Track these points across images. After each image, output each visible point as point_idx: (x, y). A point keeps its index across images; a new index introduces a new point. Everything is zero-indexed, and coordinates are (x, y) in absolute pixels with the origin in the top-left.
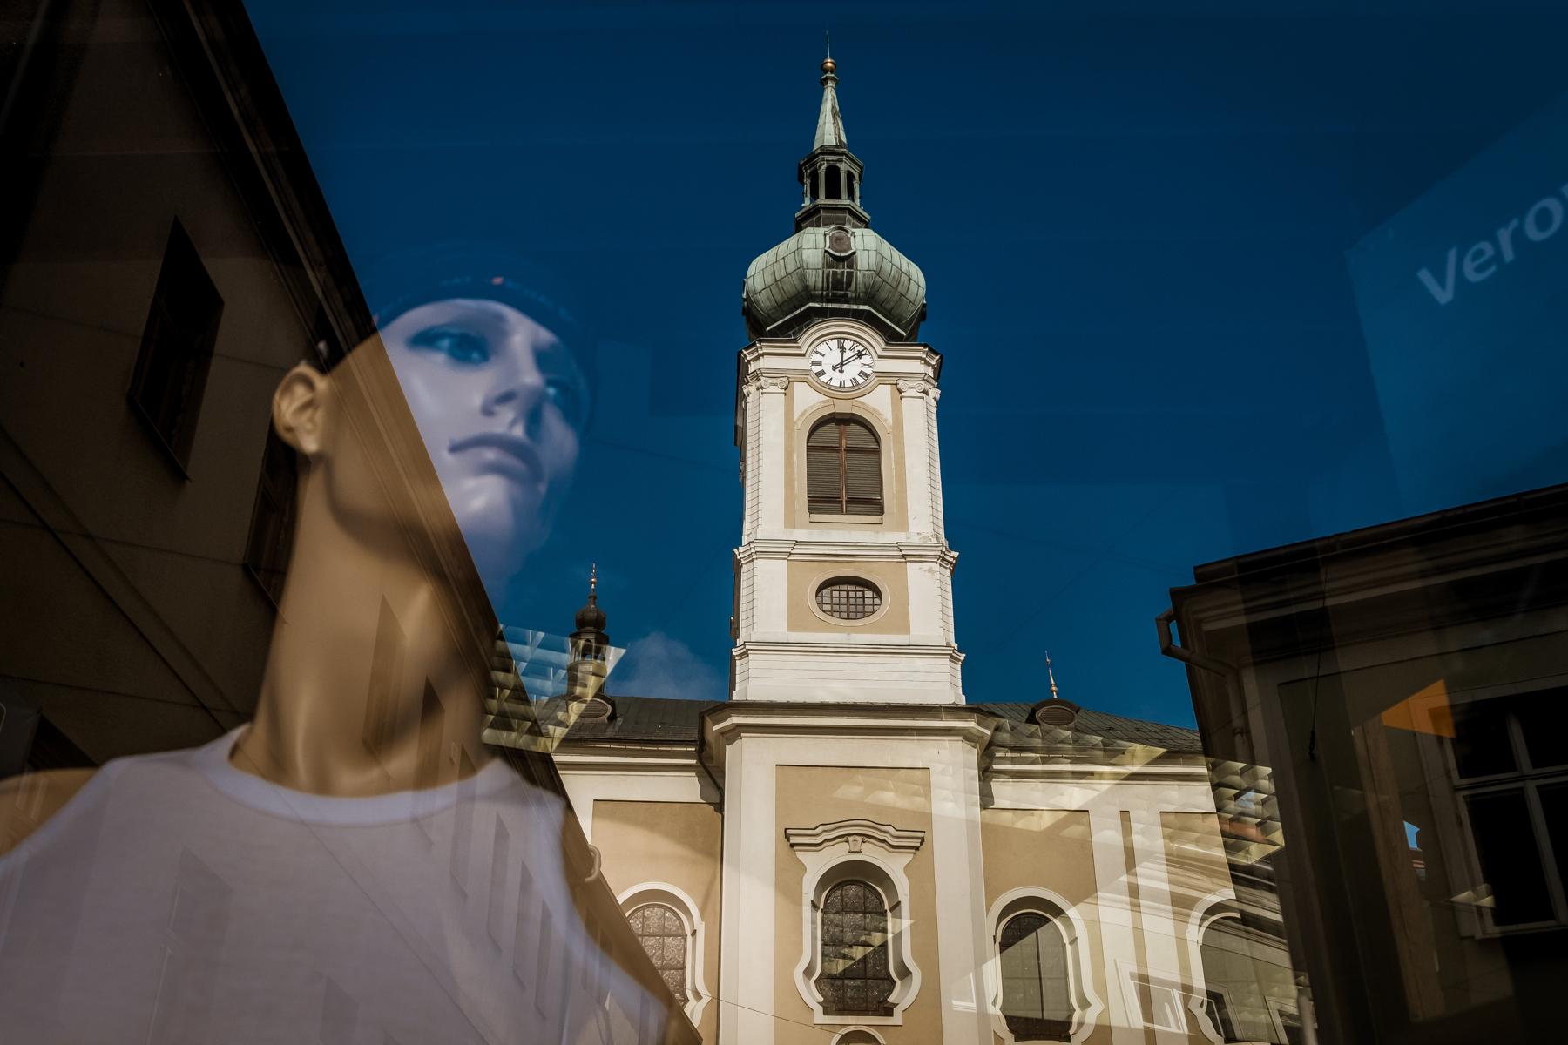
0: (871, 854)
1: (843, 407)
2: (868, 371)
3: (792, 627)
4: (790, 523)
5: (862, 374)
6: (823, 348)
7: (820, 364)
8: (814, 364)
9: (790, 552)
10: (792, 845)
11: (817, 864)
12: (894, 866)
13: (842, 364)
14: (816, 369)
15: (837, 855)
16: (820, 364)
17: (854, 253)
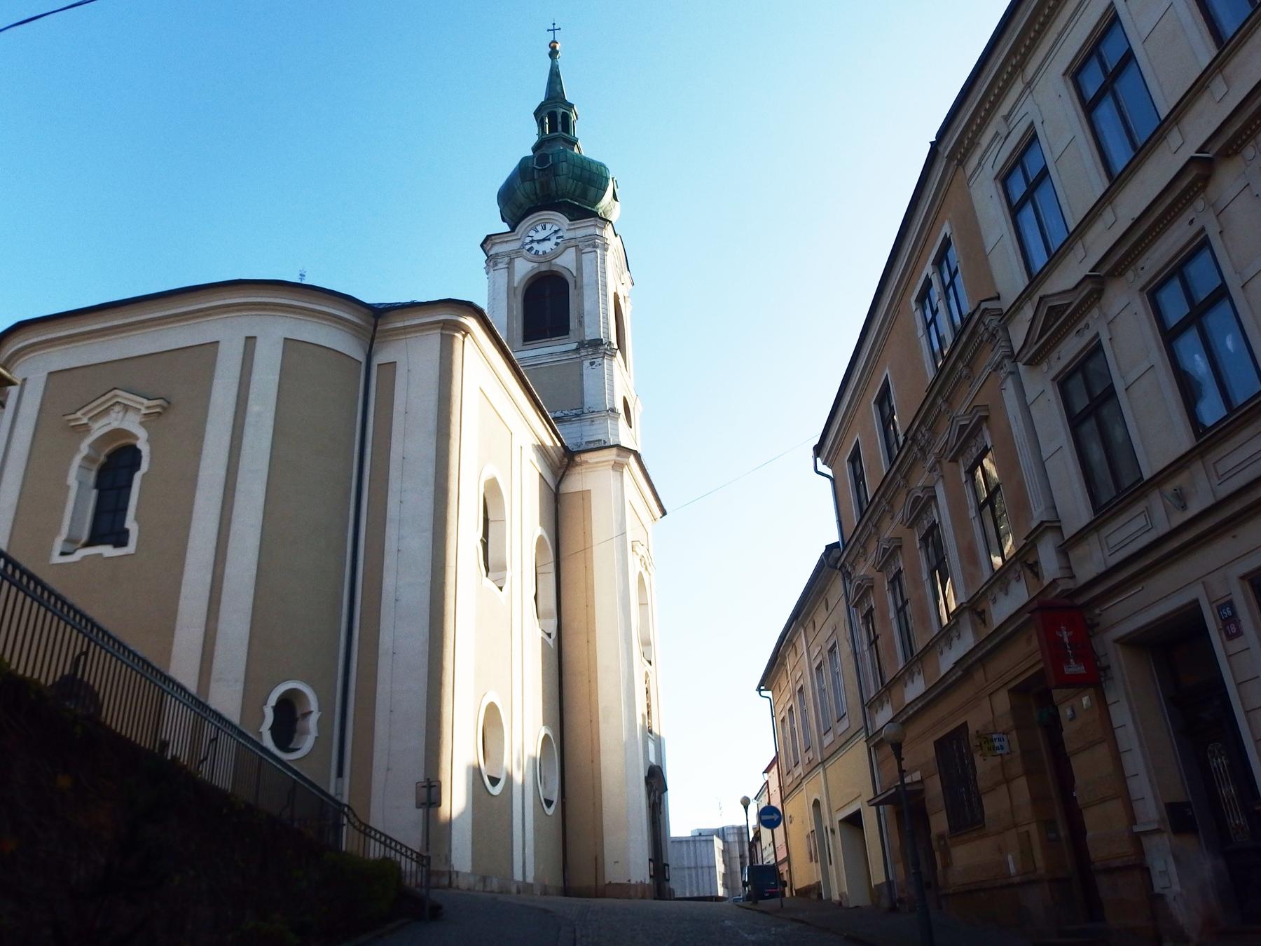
1: (544, 268)
2: (559, 241)
8: (562, 237)
16: (558, 238)
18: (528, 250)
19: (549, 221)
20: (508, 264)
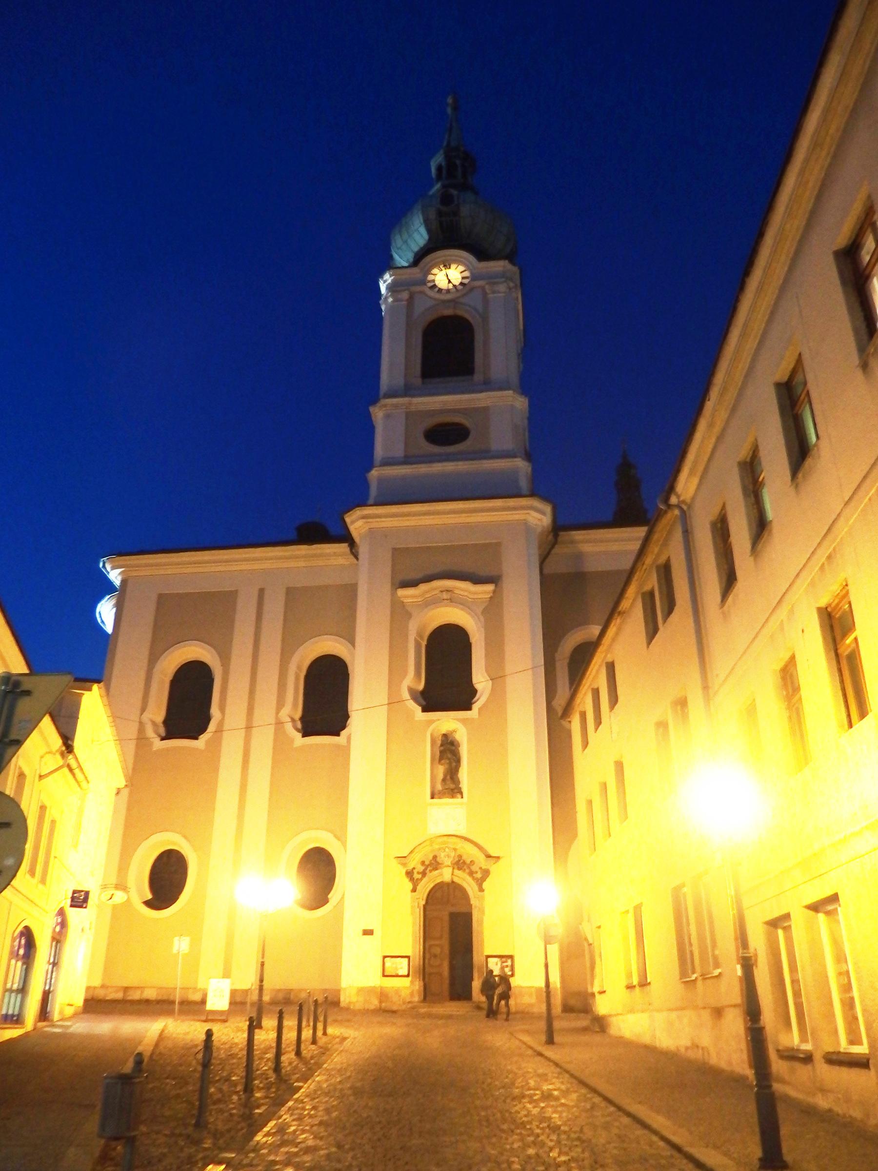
0: (605, 662)
19: (454, 258)
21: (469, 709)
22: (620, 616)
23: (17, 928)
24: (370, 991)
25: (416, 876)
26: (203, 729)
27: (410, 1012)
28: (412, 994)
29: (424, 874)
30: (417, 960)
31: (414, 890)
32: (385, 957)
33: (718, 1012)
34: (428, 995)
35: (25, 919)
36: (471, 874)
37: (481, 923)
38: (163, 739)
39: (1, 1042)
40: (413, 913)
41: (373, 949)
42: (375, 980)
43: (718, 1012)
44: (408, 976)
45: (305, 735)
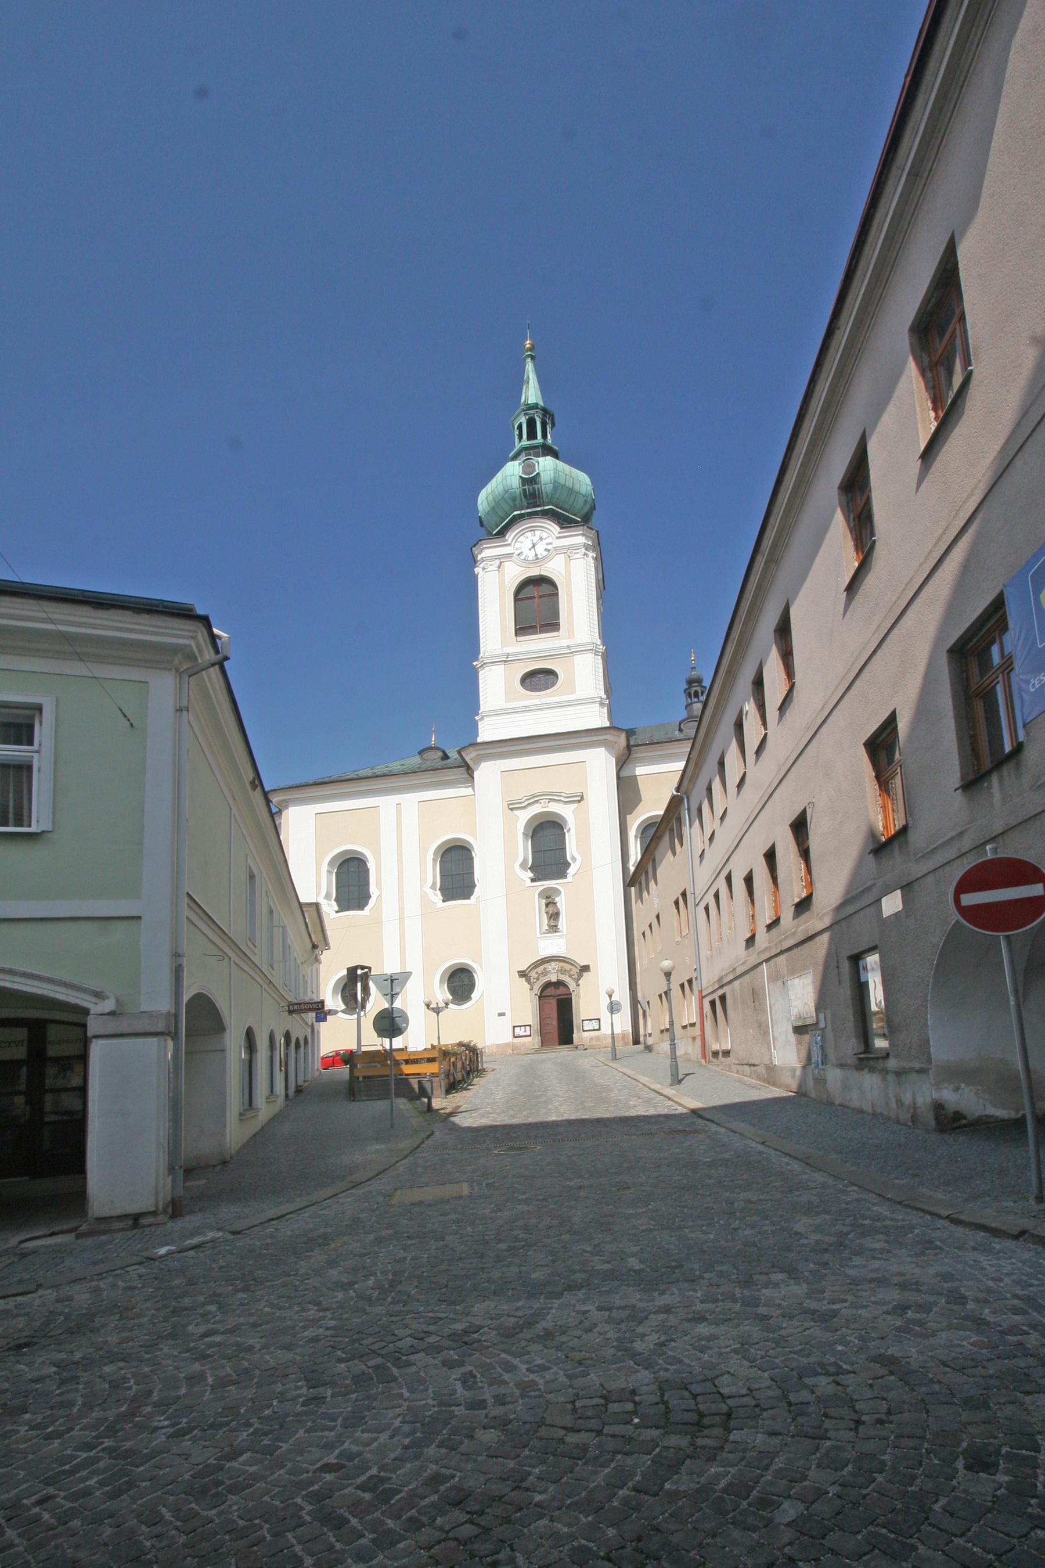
0: (554, 808)
1: (534, 572)
2: (549, 547)
3: (507, 700)
4: (504, 644)
5: (546, 550)
6: (522, 539)
7: (547, 544)
9: (506, 661)
10: (512, 809)
11: (524, 816)
12: (566, 812)
13: (534, 546)
14: (518, 552)
15: (536, 809)
16: (547, 544)
17: (538, 474)
18: (519, 555)
20: (499, 567)
21: (566, 877)
22: (169, 1199)
23: (205, 935)
24: (507, 1045)
25: (532, 980)
26: (366, 904)
27: (536, 1052)
28: (534, 1045)
29: (538, 979)
30: (536, 1026)
31: (531, 989)
32: (514, 1027)
33: (694, 1039)
34: (544, 1043)
35: (120, 709)
36: (570, 976)
37: (578, 1003)
38: (337, 912)
39: (2, 1019)
40: (531, 1001)
41: (507, 1023)
42: (508, 1038)
43: (694, 1039)
44: (530, 1036)
45: (444, 901)
